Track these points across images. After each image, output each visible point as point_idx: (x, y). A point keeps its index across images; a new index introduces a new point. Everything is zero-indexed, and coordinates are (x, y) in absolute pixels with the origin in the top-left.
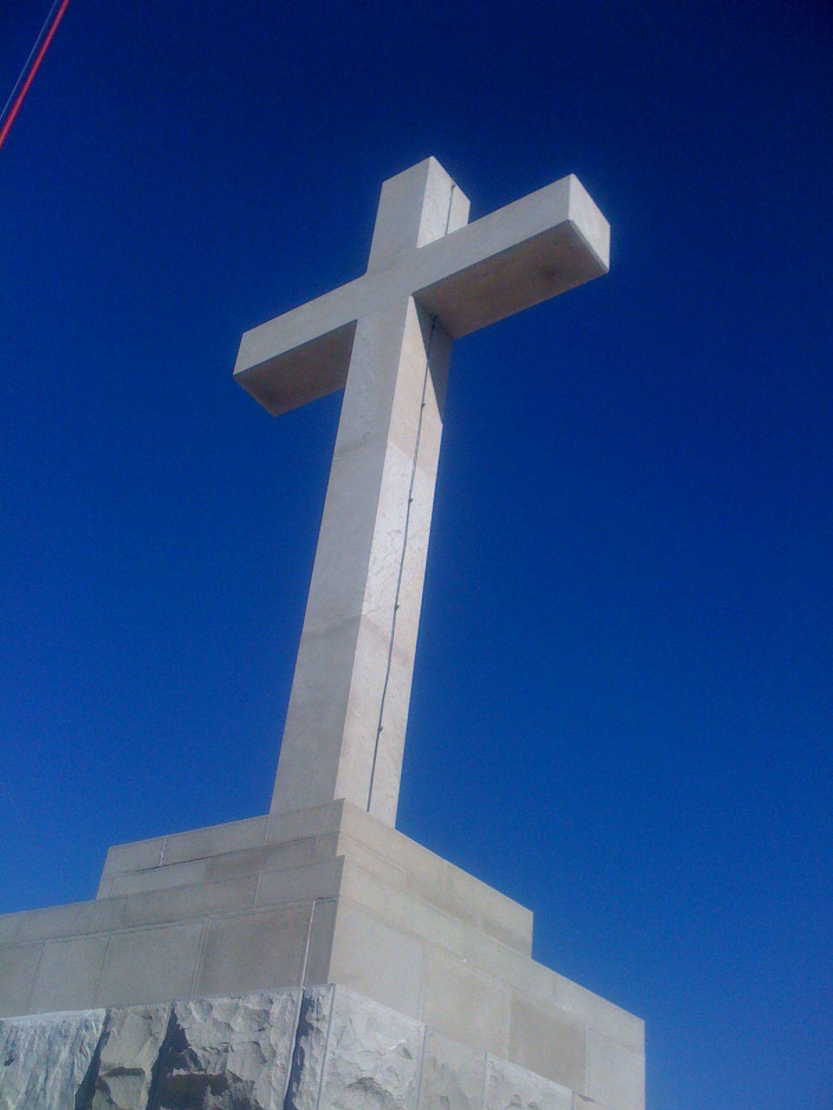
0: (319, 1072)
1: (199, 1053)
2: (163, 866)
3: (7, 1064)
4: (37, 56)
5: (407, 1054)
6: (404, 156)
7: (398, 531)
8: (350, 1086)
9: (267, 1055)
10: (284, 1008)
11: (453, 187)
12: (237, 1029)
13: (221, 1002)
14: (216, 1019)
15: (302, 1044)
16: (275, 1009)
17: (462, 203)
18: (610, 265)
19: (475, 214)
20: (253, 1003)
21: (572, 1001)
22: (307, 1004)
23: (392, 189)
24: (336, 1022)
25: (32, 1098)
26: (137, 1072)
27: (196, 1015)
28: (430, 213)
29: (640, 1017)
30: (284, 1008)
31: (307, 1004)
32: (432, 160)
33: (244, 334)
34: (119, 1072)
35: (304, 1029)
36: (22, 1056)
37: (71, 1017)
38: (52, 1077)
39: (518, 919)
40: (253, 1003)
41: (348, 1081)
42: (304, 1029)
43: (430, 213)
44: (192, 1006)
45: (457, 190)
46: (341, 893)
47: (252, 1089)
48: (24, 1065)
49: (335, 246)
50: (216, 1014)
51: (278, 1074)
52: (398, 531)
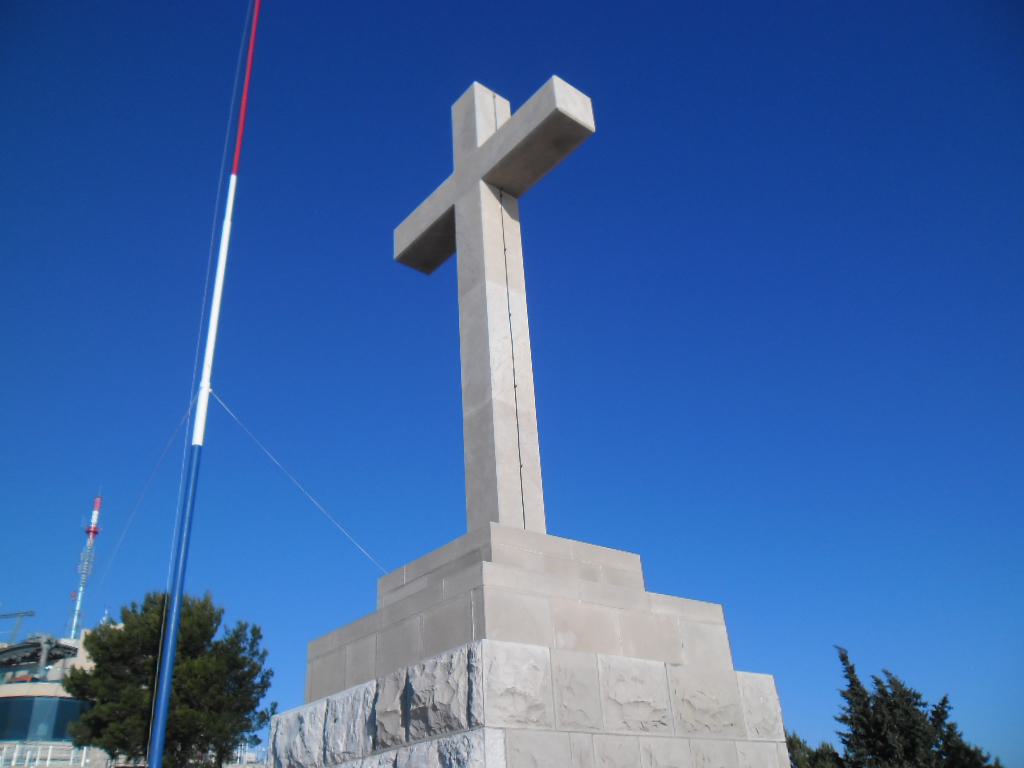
0: (481, 691)
1: (420, 694)
2: (407, 583)
3: (335, 721)
4: (244, 79)
5: (535, 668)
6: (463, 86)
7: (506, 338)
8: (502, 695)
9: (454, 687)
10: (459, 658)
11: (494, 97)
12: (437, 676)
13: (429, 663)
14: (258, 704)
15: (472, 678)
16: (455, 661)
17: (504, 105)
18: (597, 123)
19: (514, 109)
20: (444, 659)
21: (665, 608)
22: (470, 655)
23: (457, 109)
24: (486, 661)
25: (8, 760)
26: (396, 712)
27: (417, 672)
28: (487, 117)
29: (716, 603)
30: (459, 659)
31: (470, 655)
32: (476, 85)
33: (508, 102)
34: (386, 713)
35: (470, 668)
36: (340, 717)
37: (361, 689)
38: (356, 724)
39: (630, 564)
40: (444, 659)
41: (499, 693)
42: (470, 668)
43: (487, 117)
44: (416, 668)
45: (498, 97)
46: (485, 583)
47: (450, 708)
48: (343, 721)
49: (433, 156)
50: (427, 670)
51: (462, 697)
52: (506, 338)
